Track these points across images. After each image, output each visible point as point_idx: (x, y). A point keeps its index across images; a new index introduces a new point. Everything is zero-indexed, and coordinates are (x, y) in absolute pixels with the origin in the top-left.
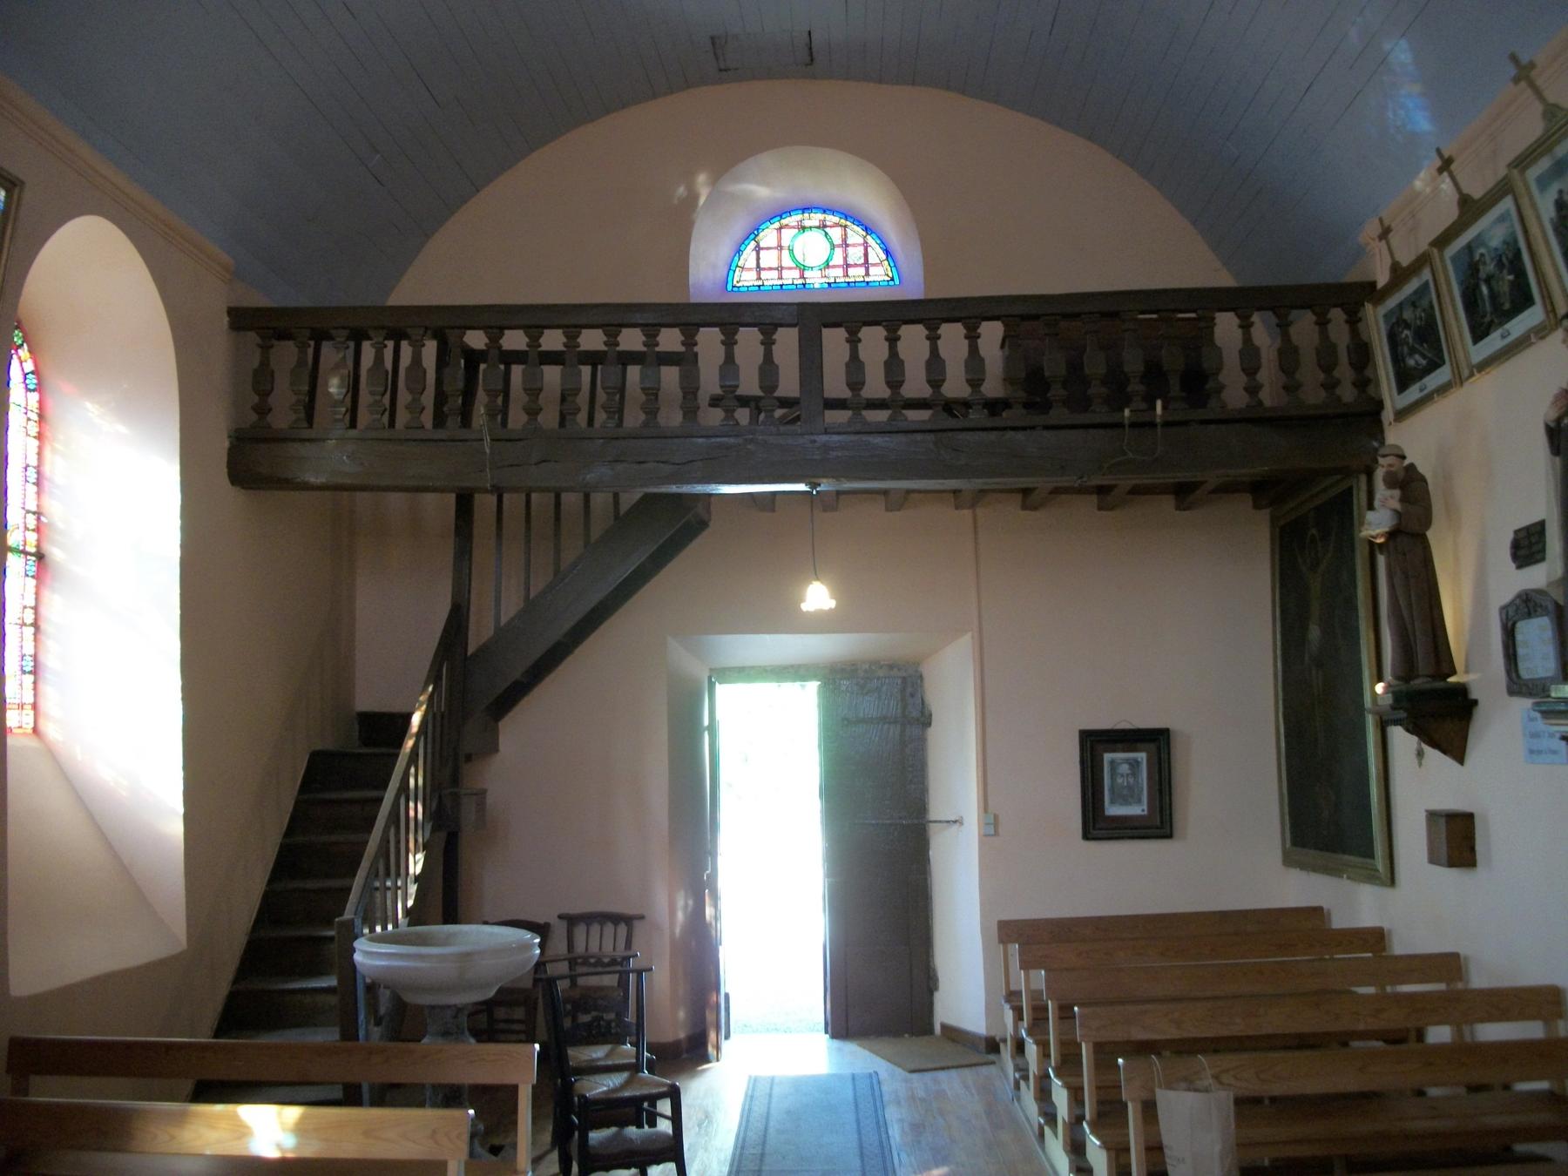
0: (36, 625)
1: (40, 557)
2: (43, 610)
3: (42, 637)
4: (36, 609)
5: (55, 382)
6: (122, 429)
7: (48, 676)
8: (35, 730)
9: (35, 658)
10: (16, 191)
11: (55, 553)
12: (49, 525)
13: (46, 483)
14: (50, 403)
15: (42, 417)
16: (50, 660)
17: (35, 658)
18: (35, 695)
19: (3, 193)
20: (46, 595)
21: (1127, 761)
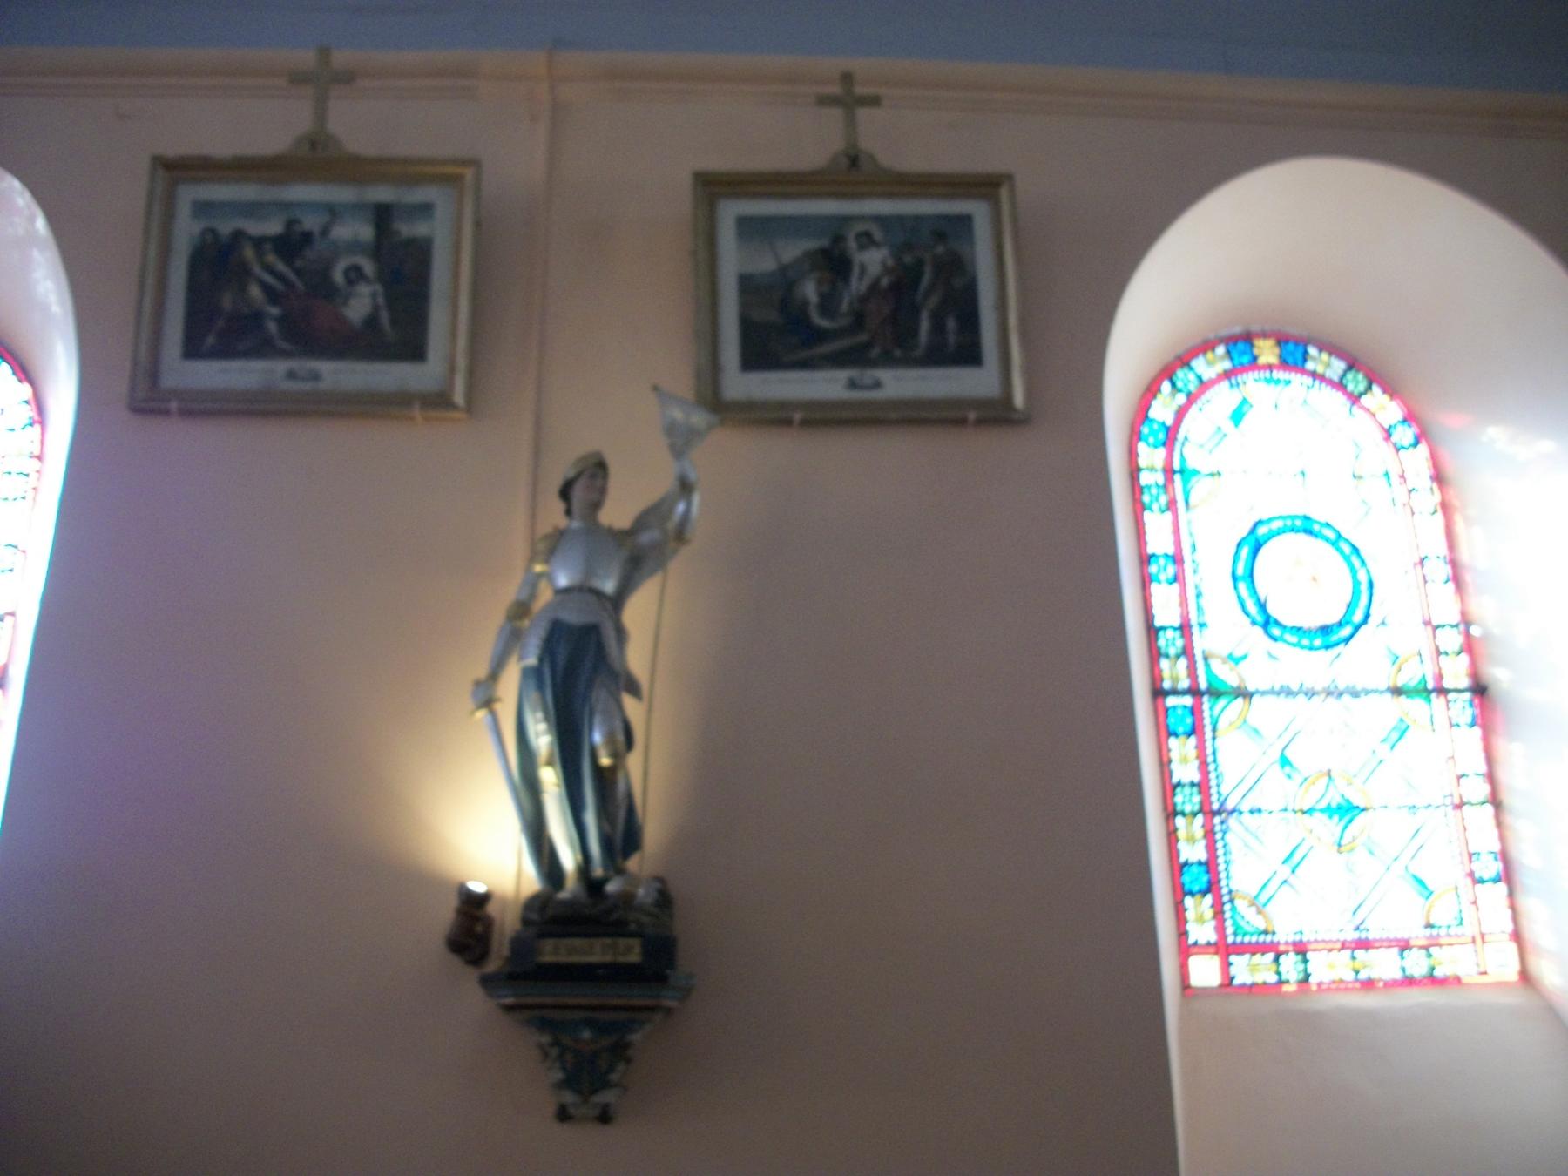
0: (1495, 801)
1: (1479, 690)
2: (1503, 775)
3: (1508, 819)
4: (1491, 777)
5: (1448, 421)
6: (1547, 446)
7: (1524, 878)
8: (1525, 976)
9: (1504, 857)
10: (1004, 193)
11: (1498, 675)
12: (1486, 636)
13: (1468, 578)
14: (1445, 455)
15: (1439, 477)
16: (1526, 856)
17: (1504, 857)
18: (1502, 838)
19: (5, 365)
20: (1503, 747)
21: (357, 208)
